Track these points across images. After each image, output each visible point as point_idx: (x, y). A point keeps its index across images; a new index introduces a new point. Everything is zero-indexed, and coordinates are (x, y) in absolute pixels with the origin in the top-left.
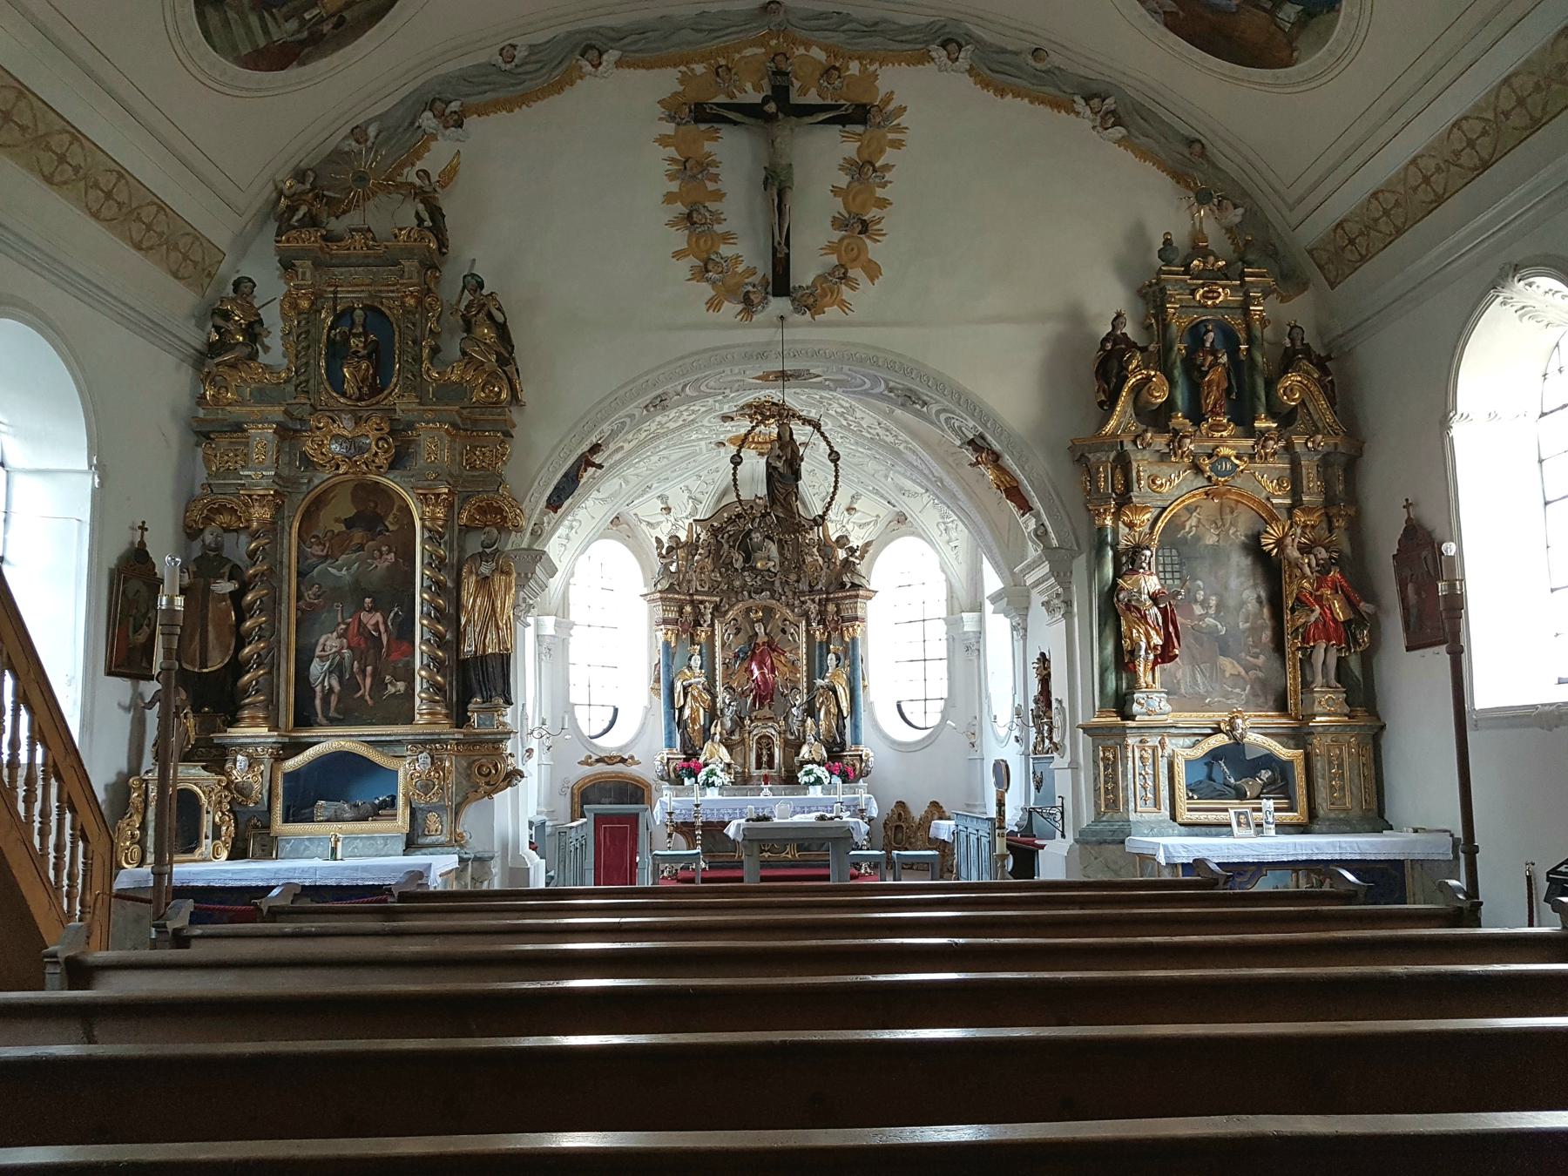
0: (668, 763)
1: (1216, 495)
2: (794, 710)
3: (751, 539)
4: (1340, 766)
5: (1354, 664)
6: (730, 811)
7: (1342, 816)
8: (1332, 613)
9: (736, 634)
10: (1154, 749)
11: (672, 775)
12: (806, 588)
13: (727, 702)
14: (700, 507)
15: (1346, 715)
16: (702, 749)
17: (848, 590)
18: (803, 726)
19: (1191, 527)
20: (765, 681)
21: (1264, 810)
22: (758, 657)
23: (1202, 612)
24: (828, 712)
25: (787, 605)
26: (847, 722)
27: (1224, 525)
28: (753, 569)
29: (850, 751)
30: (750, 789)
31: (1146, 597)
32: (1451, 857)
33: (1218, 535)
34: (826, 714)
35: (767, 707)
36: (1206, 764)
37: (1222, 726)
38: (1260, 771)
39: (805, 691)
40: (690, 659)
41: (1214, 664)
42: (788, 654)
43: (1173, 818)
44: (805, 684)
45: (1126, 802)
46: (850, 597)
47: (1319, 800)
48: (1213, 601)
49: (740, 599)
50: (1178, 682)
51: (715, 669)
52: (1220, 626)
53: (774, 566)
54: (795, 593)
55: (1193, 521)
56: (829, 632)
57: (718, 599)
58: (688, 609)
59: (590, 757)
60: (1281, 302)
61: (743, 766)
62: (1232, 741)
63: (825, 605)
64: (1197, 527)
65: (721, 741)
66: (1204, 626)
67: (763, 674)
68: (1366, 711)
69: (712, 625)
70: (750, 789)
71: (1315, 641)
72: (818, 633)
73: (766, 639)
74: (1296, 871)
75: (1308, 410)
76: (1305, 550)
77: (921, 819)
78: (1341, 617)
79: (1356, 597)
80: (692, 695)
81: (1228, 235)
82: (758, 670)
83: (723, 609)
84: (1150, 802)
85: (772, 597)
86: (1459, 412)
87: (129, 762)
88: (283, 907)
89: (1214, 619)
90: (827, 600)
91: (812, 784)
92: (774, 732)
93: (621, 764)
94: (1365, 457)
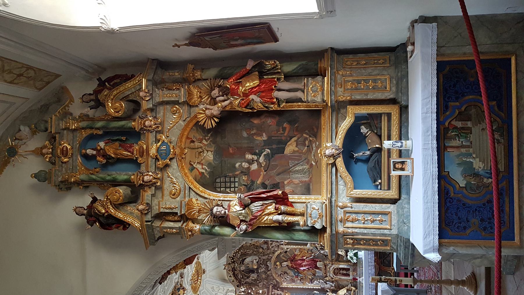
1: (182, 153)
4: (359, 82)
5: (289, 68)
7: (395, 82)
8: (255, 87)
10: (346, 212)
14: (230, 289)
15: (323, 78)
19: (203, 168)
21: (391, 147)
23: (256, 164)
27: (201, 147)
28: (257, 269)
31: (243, 211)
32: (435, 24)
33: (207, 151)
36: (356, 163)
37: (331, 162)
38: (362, 133)
41: (289, 158)
43: (394, 201)
45: (385, 235)
47: (383, 97)
48: (249, 156)
50: (301, 182)
52: (265, 153)
55: (199, 167)
57: (271, 286)
60: (73, 102)
62: (341, 155)
64: (202, 165)
66: (264, 163)
67: (305, 266)
68: (321, 61)
71: (273, 98)
74: (445, 148)
75: (130, 94)
76: (214, 102)
78: (257, 82)
79: (243, 71)
81: (37, 133)
83: (275, 283)
84: (384, 218)
85: (270, 260)
86: (100, 25)
89: (260, 156)
91: (357, 257)
94: (157, 57)
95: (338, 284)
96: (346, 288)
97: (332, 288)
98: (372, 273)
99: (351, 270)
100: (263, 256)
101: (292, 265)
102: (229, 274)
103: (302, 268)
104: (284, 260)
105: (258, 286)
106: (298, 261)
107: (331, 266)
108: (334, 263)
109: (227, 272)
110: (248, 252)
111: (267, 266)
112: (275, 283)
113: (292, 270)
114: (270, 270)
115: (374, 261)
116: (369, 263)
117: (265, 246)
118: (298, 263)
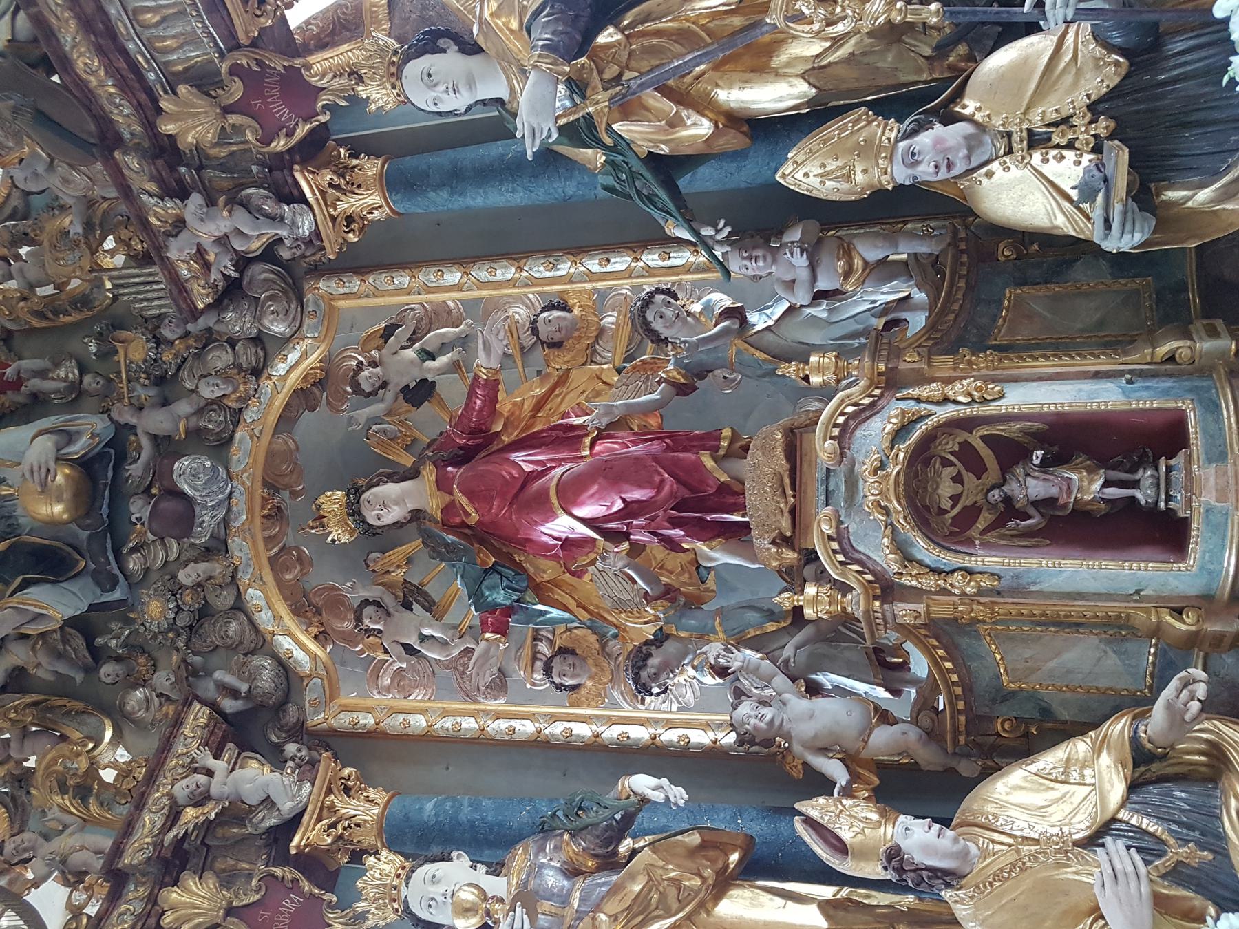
9: (430, 606)
44: (619, 263)
72: (347, 205)
73: (429, 473)
82: (550, 515)
85: (220, 446)
88: (916, 645)
92: (879, 428)
95: (968, 688)
96: (1118, 727)
97: (882, 737)
103: (562, 526)
108: (910, 361)
110: (36, 384)
111: (168, 505)
112: (266, 680)
118: (506, 472)
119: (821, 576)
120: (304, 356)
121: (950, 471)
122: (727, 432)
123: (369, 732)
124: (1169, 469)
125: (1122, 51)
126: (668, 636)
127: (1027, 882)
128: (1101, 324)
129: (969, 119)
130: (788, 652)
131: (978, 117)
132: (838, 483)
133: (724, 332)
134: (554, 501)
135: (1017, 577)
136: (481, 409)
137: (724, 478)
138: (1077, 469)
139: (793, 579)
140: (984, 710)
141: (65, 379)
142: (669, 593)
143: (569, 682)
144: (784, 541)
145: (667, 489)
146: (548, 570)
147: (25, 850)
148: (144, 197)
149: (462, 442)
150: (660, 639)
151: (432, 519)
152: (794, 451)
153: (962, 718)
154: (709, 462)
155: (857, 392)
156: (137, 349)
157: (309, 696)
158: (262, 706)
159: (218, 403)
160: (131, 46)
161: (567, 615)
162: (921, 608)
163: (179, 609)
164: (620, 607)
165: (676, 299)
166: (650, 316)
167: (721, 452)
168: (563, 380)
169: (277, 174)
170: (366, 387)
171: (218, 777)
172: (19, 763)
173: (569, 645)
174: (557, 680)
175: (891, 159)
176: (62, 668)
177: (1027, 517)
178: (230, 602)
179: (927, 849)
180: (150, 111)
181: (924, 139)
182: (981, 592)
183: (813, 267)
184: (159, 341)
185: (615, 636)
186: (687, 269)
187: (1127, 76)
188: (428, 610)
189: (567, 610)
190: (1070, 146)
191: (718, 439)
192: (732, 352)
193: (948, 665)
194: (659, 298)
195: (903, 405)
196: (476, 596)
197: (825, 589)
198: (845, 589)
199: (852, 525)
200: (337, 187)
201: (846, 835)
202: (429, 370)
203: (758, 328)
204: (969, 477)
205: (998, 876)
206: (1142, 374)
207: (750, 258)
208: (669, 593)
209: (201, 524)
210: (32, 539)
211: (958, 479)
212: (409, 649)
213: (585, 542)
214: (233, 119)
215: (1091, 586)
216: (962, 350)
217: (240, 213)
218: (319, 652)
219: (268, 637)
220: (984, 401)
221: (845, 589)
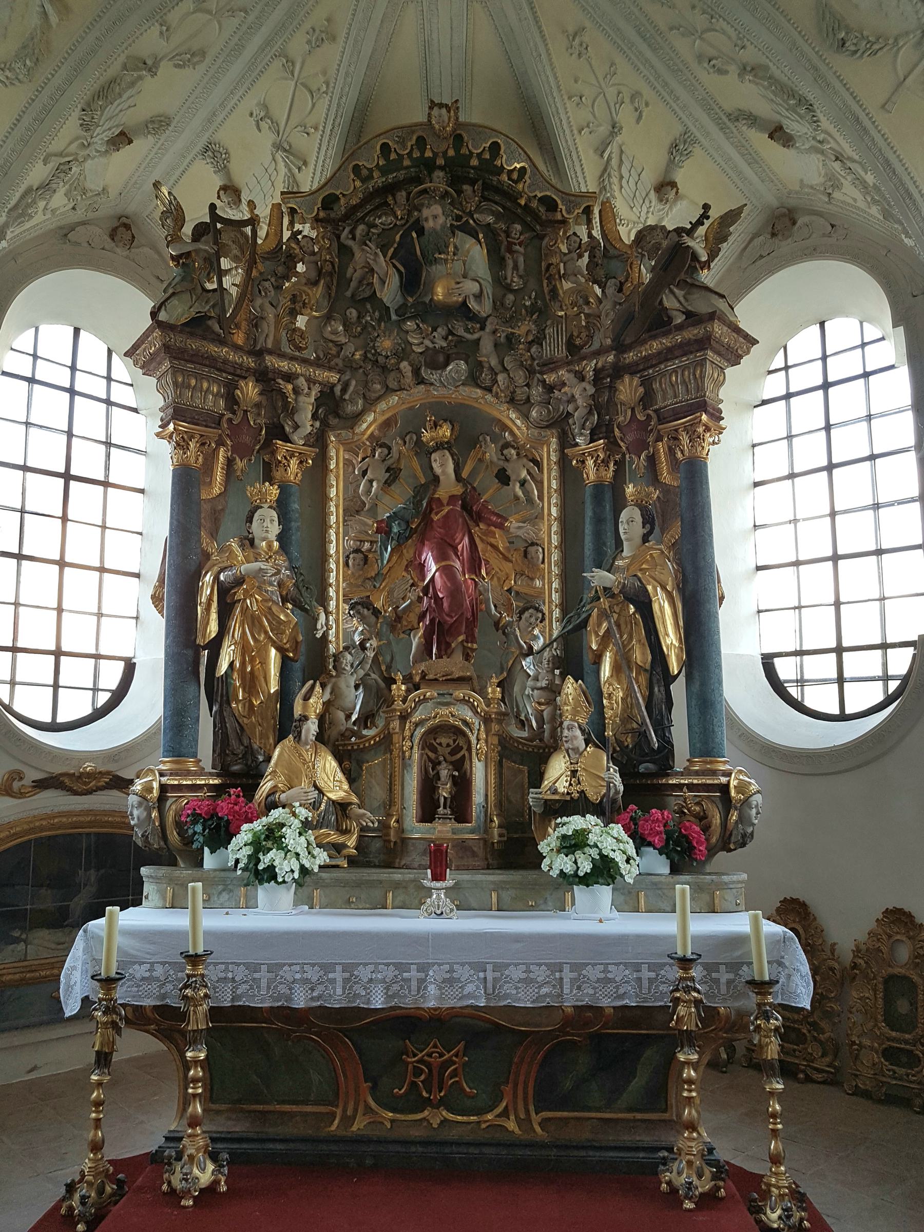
0: (162, 799)
2: (527, 664)
3: (421, 232)
6: (313, 974)
9: (388, 483)
11: (174, 836)
12: (561, 353)
13: (357, 639)
16: (268, 759)
17: (680, 328)
18: (551, 702)
20: (455, 591)
22: (438, 532)
24: (622, 666)
25: (512, 401)
26: (678, 689)
29: (687, 772)
30: (397, 886)
34: (617, 669)
35: (458, 657)
39: (557, 613)
40: (250, 520)
42: (513, 524)
46: (685, 349)
49: (393, 384)
51: (324, 557)
53: (479, 297)
54: (531, 372)
56: (620, 465)
57: (334, 377)
58: (250, 390)
59: (19, 775)
61: (390, 804)
63: (612, 389)
65: (321, 738)
67: (447, 571)
69: (319, 441)
70: (397, 886)
72: (590, 462)
73: (458, 490)
77: (857, 951)
80: (245, 610)
82: (437, 561)
85: (473, 379)
87: (849, 715)
90: (618, 371)
91: (586, 880)
92: (468, 715)
93: (115, 793)
95: (362, 750)
96: (355, 799)
97: (341, 715)
98: (508, 989)
99: (461, 831)
100: (496, 345)
101: (442, 505)
102: (402, 142)
104: (465, 463)
105: (328, 318)
106: (466, 539)
107: (476, 712)
108: (495, 727)
109: (411, 128)
110: (510, 263)
111: (441, 358)
112: (350, 409)
113: (417, 504)
114: (421, 381)
115: (586, 1001)
116: (576, 967)
117: (554, 348)
118: (459, 536)
119: (408, 691)
120: (519, 428)
121: (451, 742)
122: (475, 646)
123: (327, 466)
124: (450, 819)
125: (601, 801)
126: (377, 618)
127: (301, 765)
128: (510, 802)
129: (585, 749)
130: (373, 676)
131: (586, 753)
132: (447, 699)
133: (521, 647)
134: (443, 563)
135: (410, 765)
136: (490, 520)
137: (453, 645)
138: (451, 788)
139: (407, 679)
140: (353, 756)
141: (512, 281)
142: (398, 618)
143: (350, 563)
144: (424, 675)
145: (448, 619)
146: (408, 554)
147: (266, 293)
148: (595, 361)
149: (474, 508)
150: (376, 613)
151: (435, 492)
152: (462, 680)
153: (349, 748)
154: (461, 638)
155: (482, 706)
156: (524, 329)
157: (343, 432)
158: (337, 406)
159: (495, 381)
160: (663, 367)
161: (385, 562)
162: (397, 730)
163: (387, 357)
164: (391, 592)
165: (541, 622)
166: (531, 611)
167: (465, 644)
168: (506, 559)
169: (604, 429)
170: (505, 452)
171: (307, 400)
172: (302, 260)
173: (369, 562)
174: (351, 556)
175: (571, 720)
176: (353, 284)
177: (433, 770)
178: (390, 386)
179: (308, 730)
180: (632, 369)
181: (578, 733)
182: (404, 752)
183: (541, 688)
184: (530, 343)
185: (375, 587)
186: (551, 629)
187: (593, 804)
188: (386, 482)
189: (388, 562)
190: (571, 784)
191: (472, 642)
192: (513, 649)
193: (367, 745)
194: (540, 615)
195: (477, 724)
196: (394, 517)
197: (403, 693)
198: (404, 701)
199: (430, 704)
200: (597, 459)
201: (311, 701)
202: (514, 486)
203: (524, 663)
204: (449, 749)
205: (300, 755)
206: (486, 811)
207: (549, 661)
208: (398, 618)
209: (431, 373)
210: (424, 274)
211: (448, 745)
212: (364, 473)
213: (423, 578)
214: (629, 412)
215: (406, 792)
216: (499, 748)
217: (586, 411)
218: (366, 436)
219: (373, 409)
220: (477, 754)
221: (404, 701)
